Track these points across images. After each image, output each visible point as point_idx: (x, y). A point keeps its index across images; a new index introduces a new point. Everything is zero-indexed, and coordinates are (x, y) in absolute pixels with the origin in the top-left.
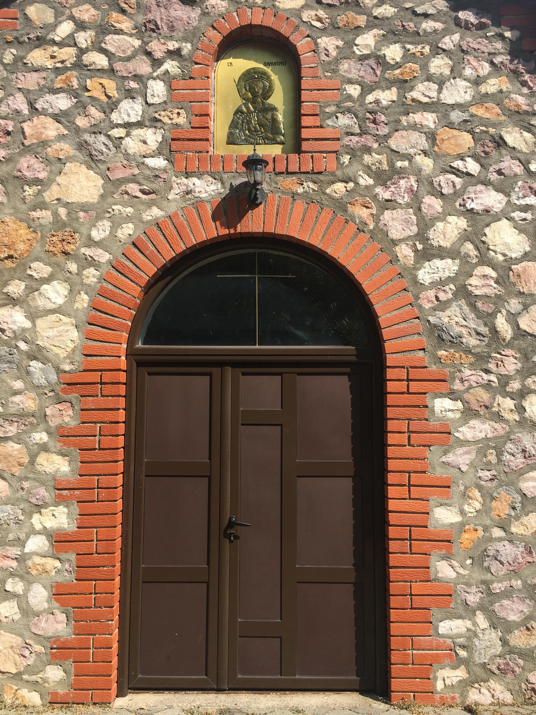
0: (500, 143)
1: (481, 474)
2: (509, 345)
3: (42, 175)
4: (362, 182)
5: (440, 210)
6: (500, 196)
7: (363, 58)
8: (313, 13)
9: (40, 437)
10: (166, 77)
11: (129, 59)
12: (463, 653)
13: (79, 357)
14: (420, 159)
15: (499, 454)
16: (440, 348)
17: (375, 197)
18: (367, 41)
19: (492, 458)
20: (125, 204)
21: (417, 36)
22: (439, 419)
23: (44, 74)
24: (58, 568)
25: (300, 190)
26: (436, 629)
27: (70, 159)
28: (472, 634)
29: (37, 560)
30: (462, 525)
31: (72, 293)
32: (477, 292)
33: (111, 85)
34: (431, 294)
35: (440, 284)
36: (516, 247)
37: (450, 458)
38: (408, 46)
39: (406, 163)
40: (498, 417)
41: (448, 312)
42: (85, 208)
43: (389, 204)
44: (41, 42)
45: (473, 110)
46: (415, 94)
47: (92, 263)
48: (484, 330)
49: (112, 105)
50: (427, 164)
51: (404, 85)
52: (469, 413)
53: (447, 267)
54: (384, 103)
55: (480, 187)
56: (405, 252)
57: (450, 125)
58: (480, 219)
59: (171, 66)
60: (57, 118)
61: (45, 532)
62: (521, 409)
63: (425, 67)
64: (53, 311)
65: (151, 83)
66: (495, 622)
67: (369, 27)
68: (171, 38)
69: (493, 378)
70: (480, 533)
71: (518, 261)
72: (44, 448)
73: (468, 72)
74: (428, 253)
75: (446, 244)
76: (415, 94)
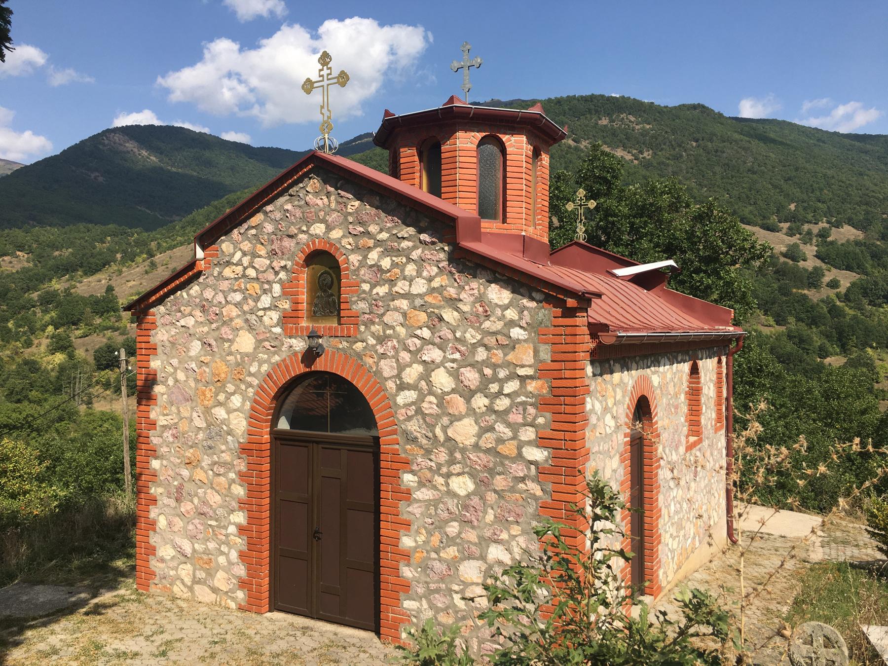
0: (441, 319)
1: (427, 520)
2: (442, 445)
3: (230, 337)
4: (369, 342)
5: (409, 360)
6: (440, 353)
7: (371, 266)
8: (347, 240)
9: (232, 475)
10: (280, 282)
11: (264, 272)
12: (414, 620)
13: (246, 436)
14: (398, 328)
15: (436, 510)
16: (408, 444)
17: (376, 352)
18: (373, 256)
19: (432, 511)
20: (264, 353)
21: (398, 252)
22: (406, 486)
23: (230, 282)
24: (240, 542)
25: (341, 347)
26: (402, 604)
27: (242, 328)
28: (419, 611)
29: (232, 537)
30: (416, 548)
31: (244, 401)
32: (427, 412)
33: (257, 286)
34: (403, 411)
35: (407, 406)
36: (447, 385)
37: (410, 509)
38: (394, 258)
39: (391, 331)
40: (435, 488)
41: (411, 423)
42: (247, 355)
43: (383, 356)
44: (228, 263)
45: (426, 298)
46: (396, 289)
47: (250, 385)
48: (430, 435)
49: (257, 299)
50: (402, 331)
51: (392, 282)
52: (421, 484)
53: (410, 396)
54: (381, 294)
55: (431, 346)
56: (391, 385)
57: (415, 308)
58: (429, 367)
59: (282, 275)
60: (236, 305)
61: (234, 524)
62: (447, 484)
63: (403, 271)
64: (235, 410)
65: (274, 285)
66: (432, 606)
67: (375, 246)
68: (282, 259)
69: (433, 464)
70: (425, 554)
71: (448, 393)
72: (233, 481)
73: (425, 274)
74: (402, 387)
75: (411, 381)
76: (396, 289)
